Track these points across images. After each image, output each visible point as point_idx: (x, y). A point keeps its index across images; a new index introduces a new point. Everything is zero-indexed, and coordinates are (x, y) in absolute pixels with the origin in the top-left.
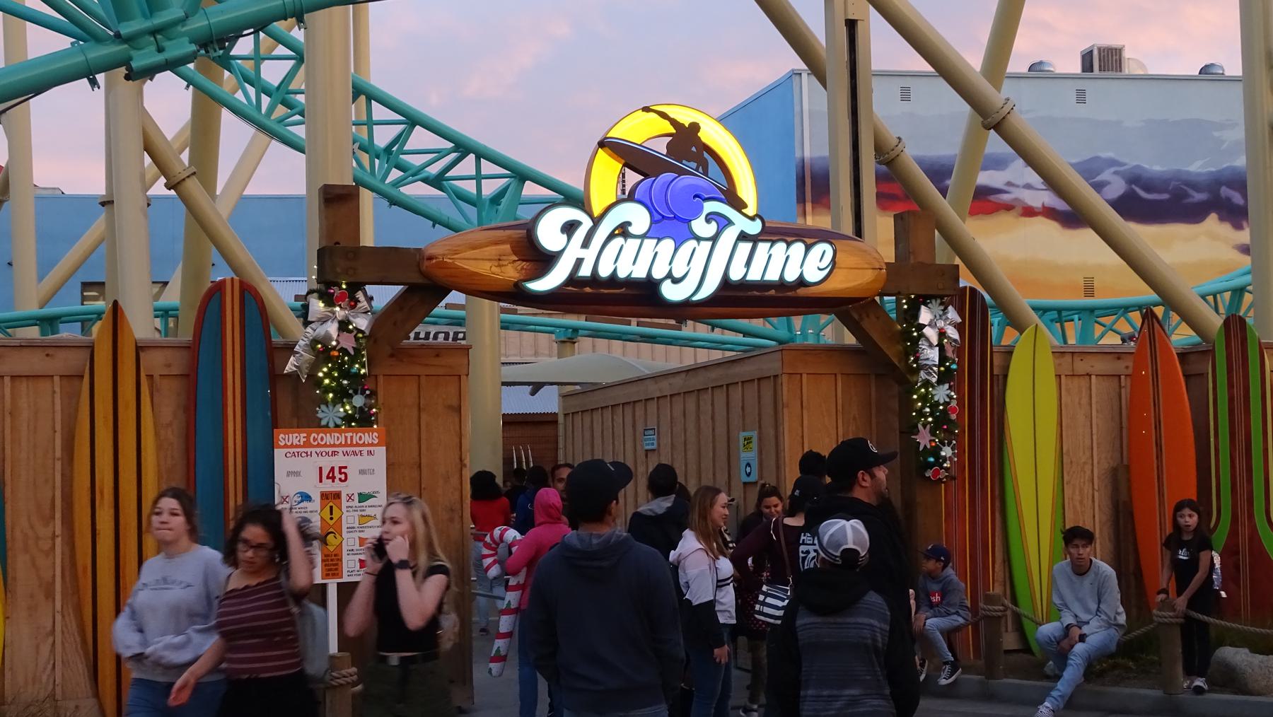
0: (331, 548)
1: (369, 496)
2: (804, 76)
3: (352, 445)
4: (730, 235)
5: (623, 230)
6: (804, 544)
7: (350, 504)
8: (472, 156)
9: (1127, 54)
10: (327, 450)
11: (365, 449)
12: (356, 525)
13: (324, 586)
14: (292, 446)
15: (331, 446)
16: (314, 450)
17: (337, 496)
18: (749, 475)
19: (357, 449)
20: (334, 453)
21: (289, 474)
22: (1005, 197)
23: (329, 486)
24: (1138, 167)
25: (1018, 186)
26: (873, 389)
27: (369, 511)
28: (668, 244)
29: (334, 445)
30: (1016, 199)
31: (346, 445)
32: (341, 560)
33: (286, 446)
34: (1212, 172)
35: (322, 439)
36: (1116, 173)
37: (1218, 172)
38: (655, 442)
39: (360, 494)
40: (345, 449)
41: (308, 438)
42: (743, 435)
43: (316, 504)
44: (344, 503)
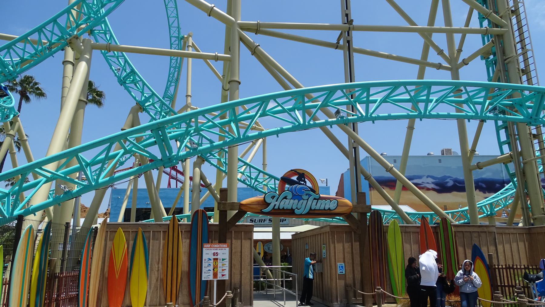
0: (215, 272)
1: (224, 259)
2: (370, 158)
3: (221, 247)
4: (311, 199)
5: (285, 198)
6: (12, 250)
7: (220, 261)
8: (273, 179)
9: (452, 151)
10: (215, 248)
11: (224, 248)
12: (221, 266)
13: (213, 281)
14: (207, 247)
15: (216, 247)
16: (212, 248)
17: (217, 259)
18: (324, 256)
19: (222, 248)
20: (217, 249)
21: (206, 254)
22: (422, 186)
23: (215, 257)
24: (456, 178)
25: (425, 183)
26: (344, 235)
27: (224, 263)
28: (296, 201)
29: (217, 247)
30: (425, 186)
31: (220, 247)
32: (217, 274)
33: (206, 247)
34: (476, 179)
35: (214, 246)
36: (450, 179)
37: (477, 179)
38: (308, 247)
39: (222, 259)
40: (219, 248)
41: (211, 245)
42: (323, 246)
43: (212, 261)
44: (219, 260)
